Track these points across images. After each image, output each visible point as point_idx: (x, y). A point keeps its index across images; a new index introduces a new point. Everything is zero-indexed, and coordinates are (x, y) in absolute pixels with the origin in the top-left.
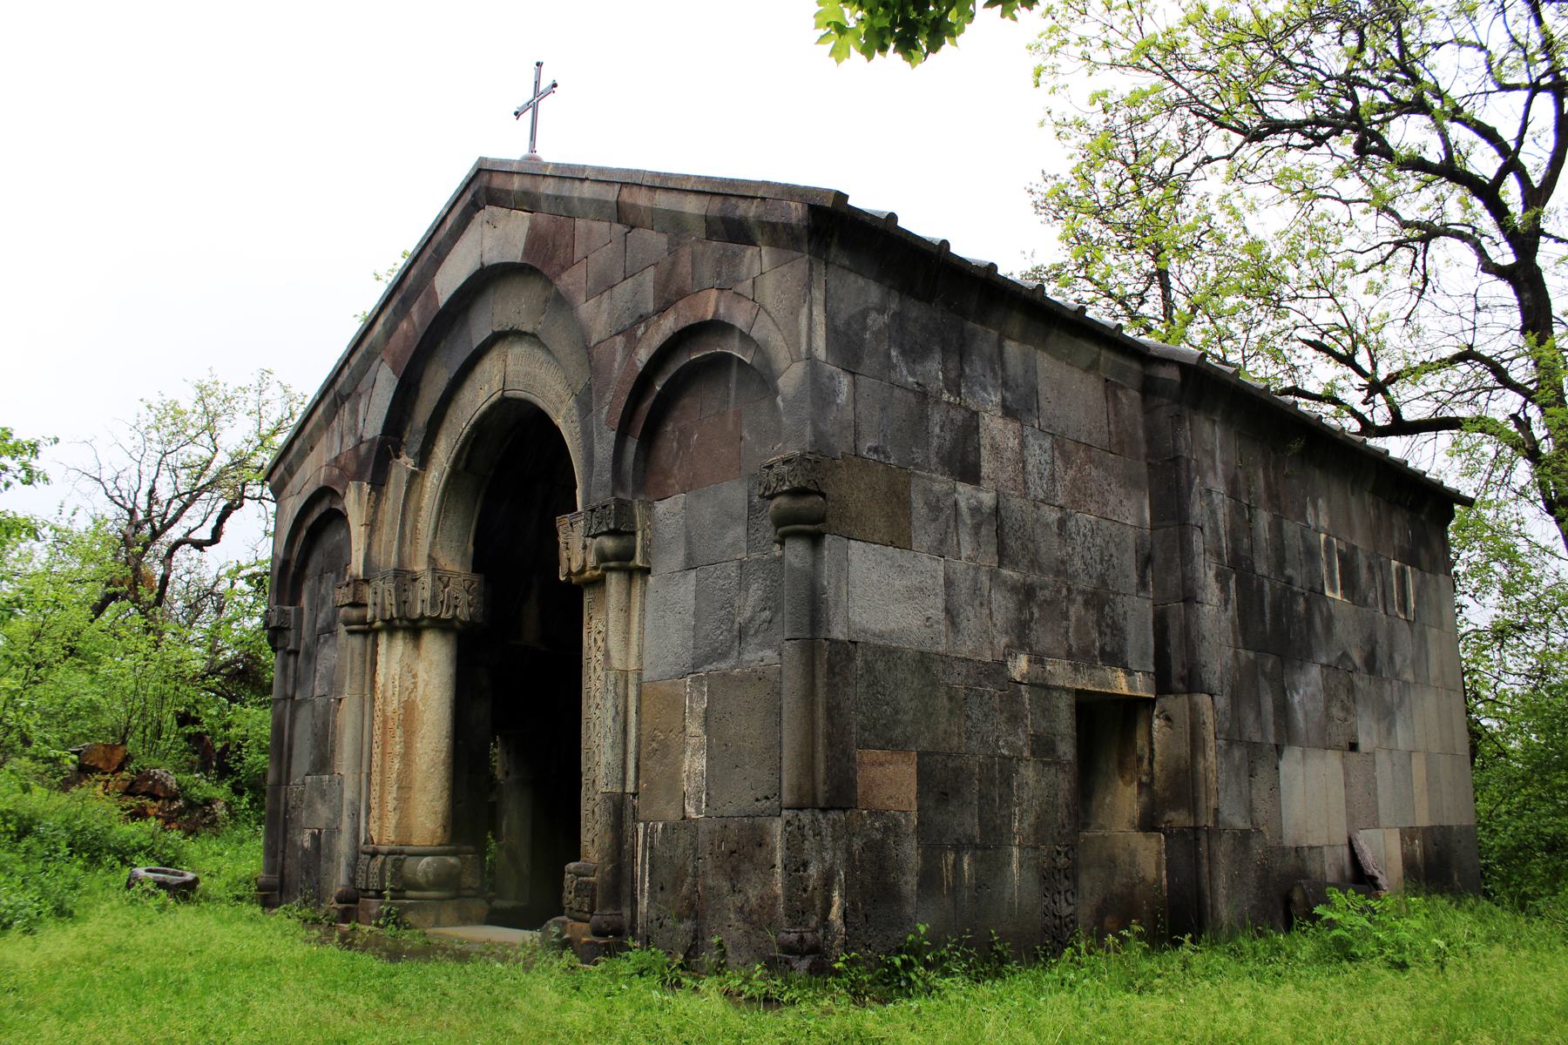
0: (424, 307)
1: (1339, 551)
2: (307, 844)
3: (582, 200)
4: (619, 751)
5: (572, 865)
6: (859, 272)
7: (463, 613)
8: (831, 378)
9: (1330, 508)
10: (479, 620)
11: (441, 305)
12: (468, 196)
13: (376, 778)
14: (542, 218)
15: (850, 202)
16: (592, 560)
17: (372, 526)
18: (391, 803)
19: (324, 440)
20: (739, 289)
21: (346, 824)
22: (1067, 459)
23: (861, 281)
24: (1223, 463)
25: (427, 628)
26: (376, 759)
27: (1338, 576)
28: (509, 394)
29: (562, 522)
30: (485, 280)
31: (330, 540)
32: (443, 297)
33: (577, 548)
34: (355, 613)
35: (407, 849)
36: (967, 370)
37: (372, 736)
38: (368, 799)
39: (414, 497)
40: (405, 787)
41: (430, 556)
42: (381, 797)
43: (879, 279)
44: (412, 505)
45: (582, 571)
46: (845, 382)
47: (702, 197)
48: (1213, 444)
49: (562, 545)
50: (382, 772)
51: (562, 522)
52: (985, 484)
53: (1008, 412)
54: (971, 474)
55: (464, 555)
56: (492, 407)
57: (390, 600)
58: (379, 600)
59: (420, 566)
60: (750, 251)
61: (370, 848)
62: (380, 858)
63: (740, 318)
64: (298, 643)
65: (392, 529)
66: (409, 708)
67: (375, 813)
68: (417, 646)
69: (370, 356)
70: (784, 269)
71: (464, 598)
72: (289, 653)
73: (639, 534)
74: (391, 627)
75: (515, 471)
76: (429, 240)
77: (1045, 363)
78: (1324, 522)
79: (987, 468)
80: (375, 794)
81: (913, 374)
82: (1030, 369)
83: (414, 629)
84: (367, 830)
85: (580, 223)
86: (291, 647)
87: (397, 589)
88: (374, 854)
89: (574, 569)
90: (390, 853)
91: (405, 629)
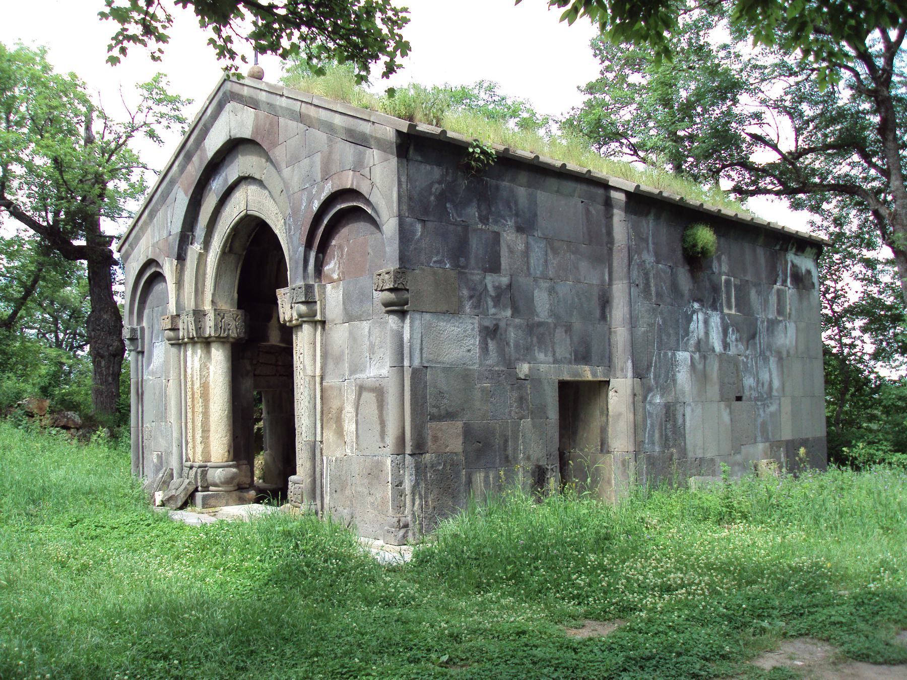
0: (201, 159)
1: (735, 286)
2: (155, 460)
3: (281, 107)
4: (312, 419)
5: (292, 478)
6: (427, 162)
7: (234, 334)
8: (411, 225)
9: (729, 259)
10: (242, 335)
11: (209, 158)
12: (220, 94)
13: (190, 425)
14: (262, 114)
15: (417, 128)
16: (295, 316)
17: (179, 284)
18: (198, 438)
19: (149, 231)
20: (362, 172)
21: (175, 450)
22: (555, 252)
23: (428, 167)
24: (654, 243)
25: (214, 342)
26: (190, 415)
27: (733, 300)
28: (249, 212)
29: (280, 293)
30: (233, 146)
31: (158, 288)
32: (210, 154)
33: (288, 307)
34: (171, 334)
35: (209, 464)
36: (493, 209)
37: (186, 402)
38: (186, 436)
39: (202, 267)
40: (206, 431)
41: (212, 301)
42: (193, 436)
43: (439, 165)
44: (201, 271)
45: (291, 321)
46: (419, 227)
47: (343, 117)
48: (648, 234)
49: (280, 305)
50: (193, 422)
51: (280, 293)
52: (503, 272)
53: (519, 229)
54: (494, 267)
55: (232, 299)
56: (242, 219)
57: (192, 327)
58: (185, 327)
59: (207, 307)
60: (369, 151)
61: (189, 464)
62: (194, 469)
63: (364, 189)
64: (143, 347)
65: (191, 286)
66: (205, 387)
67: (190, 445)
68: (209, 352)
69: (172, 183)
70: (385, 164)
71: (233, 324)
72: (138, 352)
73: (318, 303)
74: (193, 341)
75: (255, 259)
76: (200, 119)
77: (541, 196)
78: (725, 268)
79: (504, 262)
80: (190, 434)
81: (460, 215)
82: (533, 201)
83: (207, 343)
84: (187, 454)
85: (281, 120)
86: (139, 349)
87: (195, 321)
88: (191, 468)
89: (287, 319)
90: (200, 467)
91: (201, 342)
